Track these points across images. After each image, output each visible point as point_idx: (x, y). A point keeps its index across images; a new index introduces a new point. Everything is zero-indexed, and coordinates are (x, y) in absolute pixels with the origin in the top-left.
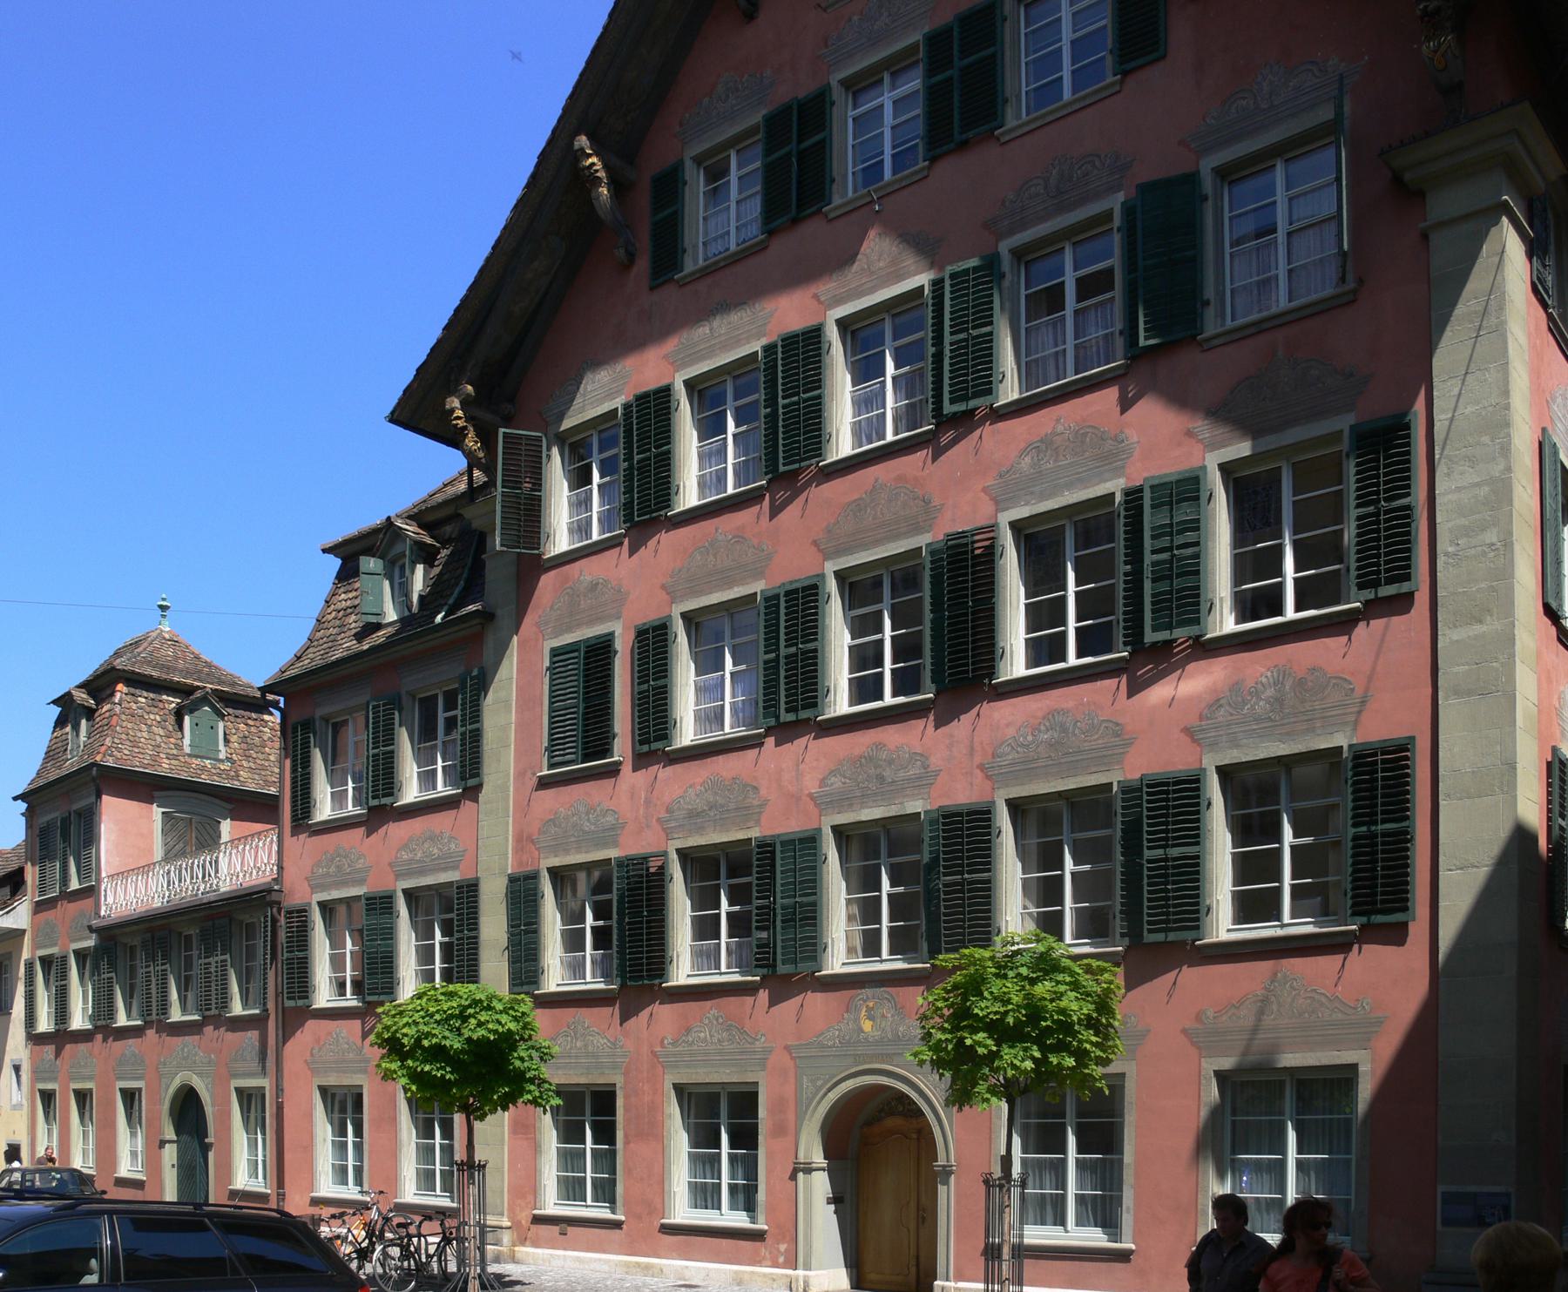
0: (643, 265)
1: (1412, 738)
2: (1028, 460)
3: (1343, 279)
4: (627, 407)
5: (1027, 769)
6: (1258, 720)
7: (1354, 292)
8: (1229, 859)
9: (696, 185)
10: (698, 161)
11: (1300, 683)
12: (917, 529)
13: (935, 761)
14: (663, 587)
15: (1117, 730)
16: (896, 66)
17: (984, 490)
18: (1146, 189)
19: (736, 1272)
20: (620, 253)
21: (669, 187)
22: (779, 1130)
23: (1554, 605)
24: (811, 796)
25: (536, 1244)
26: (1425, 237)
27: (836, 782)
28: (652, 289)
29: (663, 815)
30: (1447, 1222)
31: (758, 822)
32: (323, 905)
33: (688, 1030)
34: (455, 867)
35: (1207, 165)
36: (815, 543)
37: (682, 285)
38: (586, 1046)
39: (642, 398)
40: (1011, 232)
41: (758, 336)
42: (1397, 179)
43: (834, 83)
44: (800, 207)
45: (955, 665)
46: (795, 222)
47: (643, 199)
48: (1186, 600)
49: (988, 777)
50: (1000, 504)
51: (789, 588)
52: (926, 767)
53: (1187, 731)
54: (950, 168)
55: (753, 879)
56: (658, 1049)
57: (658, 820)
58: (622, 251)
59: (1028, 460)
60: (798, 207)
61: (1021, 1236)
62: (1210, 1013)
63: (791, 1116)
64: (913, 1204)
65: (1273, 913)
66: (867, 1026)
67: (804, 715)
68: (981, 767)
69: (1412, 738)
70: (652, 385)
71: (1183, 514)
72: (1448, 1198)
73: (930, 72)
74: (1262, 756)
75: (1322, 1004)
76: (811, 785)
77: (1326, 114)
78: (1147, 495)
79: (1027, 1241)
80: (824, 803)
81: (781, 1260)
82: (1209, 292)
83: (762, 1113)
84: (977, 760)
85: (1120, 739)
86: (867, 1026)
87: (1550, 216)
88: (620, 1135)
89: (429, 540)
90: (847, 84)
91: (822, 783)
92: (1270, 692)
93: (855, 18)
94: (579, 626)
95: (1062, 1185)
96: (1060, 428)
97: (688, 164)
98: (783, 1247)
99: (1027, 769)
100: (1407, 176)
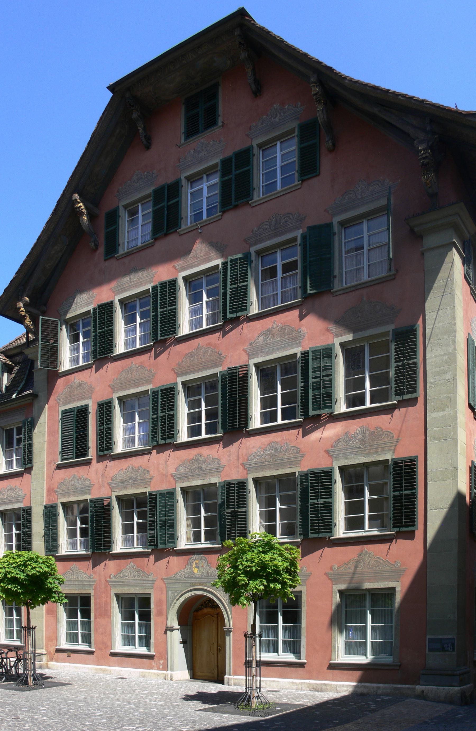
0: (101, 250)
2: (262, 338)
3: (390, 270)
7: (395, 275)
9: (124, 217)
10: (125, 207)
11: (372, 433)
15: (298, 451)
16: (209, 172)
17: (244, 350)
18: (310, 229)
19: (142, 672)
21: (113, 218)
24: (171, 475)
26: (423, 254)
27: (182, 469)
28: (105, 260)
30: (430, 650)
31: (149, 485)
33: (121, 571)
35: (336, 220)
36: (173, 370)
39: (101, 307)
40: (256, 244)
41: (150, 282)
42: (412, 231)
43: (183, 178)
46: (166, 235)
47: (102, 222)
49: (245, 469)
50: (250, 356)
53: (327, 452)
56: (108, 579)
57: (108, 483)
59: (262, 338)
60: (168, 199)
63: (164, 608)
66: (196, 570)
68: (242, 465)
69: (417, 457)
70: (105, 301)
71: (325, 363)
72: (431, 641)
73: (223, 175)
75: (381, 563)
77: (383, 202)
80: (177, 478)
81: (161, 667)
82: (336, 272)
84: (241, 461)
86: (196, 570)
90: (188, 178)
91: (176, 469)
92: (360, 436)
93: (192, 151)
94: (74, 401)
96: (275, 326)
98: (162, 662)
100: (416, 229)
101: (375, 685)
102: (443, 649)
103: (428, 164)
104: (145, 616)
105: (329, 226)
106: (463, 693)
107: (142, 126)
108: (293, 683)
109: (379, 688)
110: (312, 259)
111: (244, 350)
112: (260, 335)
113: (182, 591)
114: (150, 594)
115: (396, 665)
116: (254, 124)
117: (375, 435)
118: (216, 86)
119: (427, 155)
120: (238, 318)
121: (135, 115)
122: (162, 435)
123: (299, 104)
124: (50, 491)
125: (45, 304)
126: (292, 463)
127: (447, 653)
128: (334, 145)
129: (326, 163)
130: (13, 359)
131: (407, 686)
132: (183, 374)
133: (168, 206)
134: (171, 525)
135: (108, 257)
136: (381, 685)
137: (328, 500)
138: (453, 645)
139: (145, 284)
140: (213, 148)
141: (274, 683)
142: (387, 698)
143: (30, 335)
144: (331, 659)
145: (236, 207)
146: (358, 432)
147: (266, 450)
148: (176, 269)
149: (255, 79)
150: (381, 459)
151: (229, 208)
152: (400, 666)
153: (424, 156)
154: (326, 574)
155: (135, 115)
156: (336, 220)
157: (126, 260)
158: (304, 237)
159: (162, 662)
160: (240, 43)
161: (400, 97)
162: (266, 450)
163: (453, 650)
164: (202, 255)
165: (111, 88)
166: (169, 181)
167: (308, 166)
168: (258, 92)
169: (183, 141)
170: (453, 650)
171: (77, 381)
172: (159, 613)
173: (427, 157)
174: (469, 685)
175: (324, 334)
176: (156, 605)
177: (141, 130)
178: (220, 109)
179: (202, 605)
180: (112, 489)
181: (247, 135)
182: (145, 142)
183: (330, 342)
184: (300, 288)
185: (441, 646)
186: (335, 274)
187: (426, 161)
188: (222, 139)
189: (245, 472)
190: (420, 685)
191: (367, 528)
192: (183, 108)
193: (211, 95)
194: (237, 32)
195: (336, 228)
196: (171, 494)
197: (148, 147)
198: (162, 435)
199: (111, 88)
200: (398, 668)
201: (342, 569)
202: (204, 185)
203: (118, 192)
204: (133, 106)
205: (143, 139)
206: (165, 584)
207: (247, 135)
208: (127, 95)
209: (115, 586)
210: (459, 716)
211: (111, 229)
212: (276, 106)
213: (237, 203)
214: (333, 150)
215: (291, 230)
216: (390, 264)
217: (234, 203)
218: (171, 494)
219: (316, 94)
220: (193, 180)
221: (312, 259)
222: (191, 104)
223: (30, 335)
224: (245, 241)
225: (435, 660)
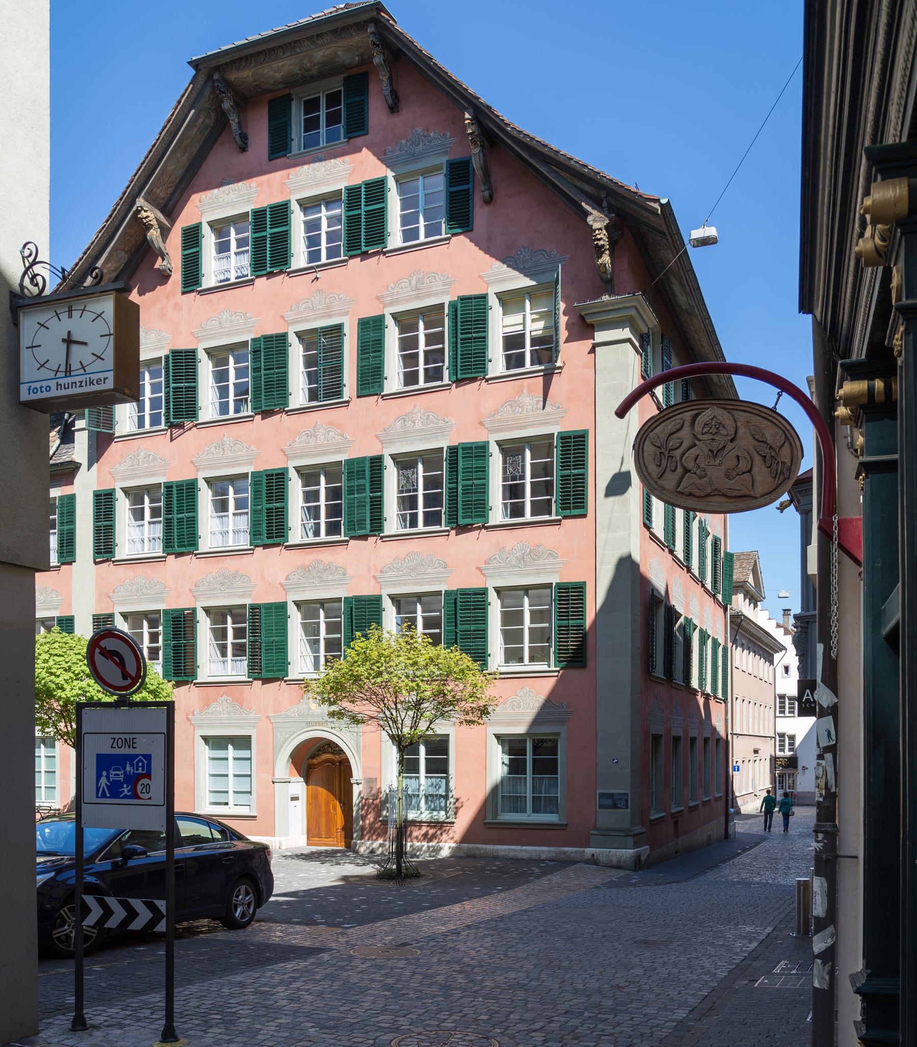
1: (585, 583)
2: (399, 424)
8: (499, 614)
12: (340, 451)
17: (376, 436)
23: (648, 522)
24: (280, 584)
26: (593, 350)
28: (183, 293)
30: (601, 807)
33: (208, 706)
48: (480, 508)
49: (379, 583)
51: (269, 473)
53: (479, 569)
55: (246, 625)
57: (190, 590)
59: (399, 424)
61: (49, 742)
65: (521, 364)
67: (277, 540)
69: (585, 583)
72: (602, 795)
78: (460, 452)
79: (42, 751)
91: (287, 578)
101: (538, 848)
102: (615, 806)
106: (638, 857)
107: (237, 120)
112: (397, 420)
113: (294, 733)
119: (602, 236)
122: (270, 529)
128: (491, 196)
131: (575, 849)
132: (296, 457)
134: (281, 648)
138: (627, 801)
142: (552, 863)
149: (391, 91)
155: (227, 105)
160: (374, 44)
162: (403, 562)
163: (627, 808)
164: (321, 307)
170: (627, 808)
175: (476, 428)
179: (319, 750)
189: (378, 587)
194: (371, 29)
196: (281, 607)
198: (270, 529)
202: (324, 214)
203: (200, 201)
204: (224, 93)
205: (238, 138)
206: (272, 723)
208: (216, 76)
209: (201, 726)
210: (634, 881)
218: (281, 607)
225: (608, 818)
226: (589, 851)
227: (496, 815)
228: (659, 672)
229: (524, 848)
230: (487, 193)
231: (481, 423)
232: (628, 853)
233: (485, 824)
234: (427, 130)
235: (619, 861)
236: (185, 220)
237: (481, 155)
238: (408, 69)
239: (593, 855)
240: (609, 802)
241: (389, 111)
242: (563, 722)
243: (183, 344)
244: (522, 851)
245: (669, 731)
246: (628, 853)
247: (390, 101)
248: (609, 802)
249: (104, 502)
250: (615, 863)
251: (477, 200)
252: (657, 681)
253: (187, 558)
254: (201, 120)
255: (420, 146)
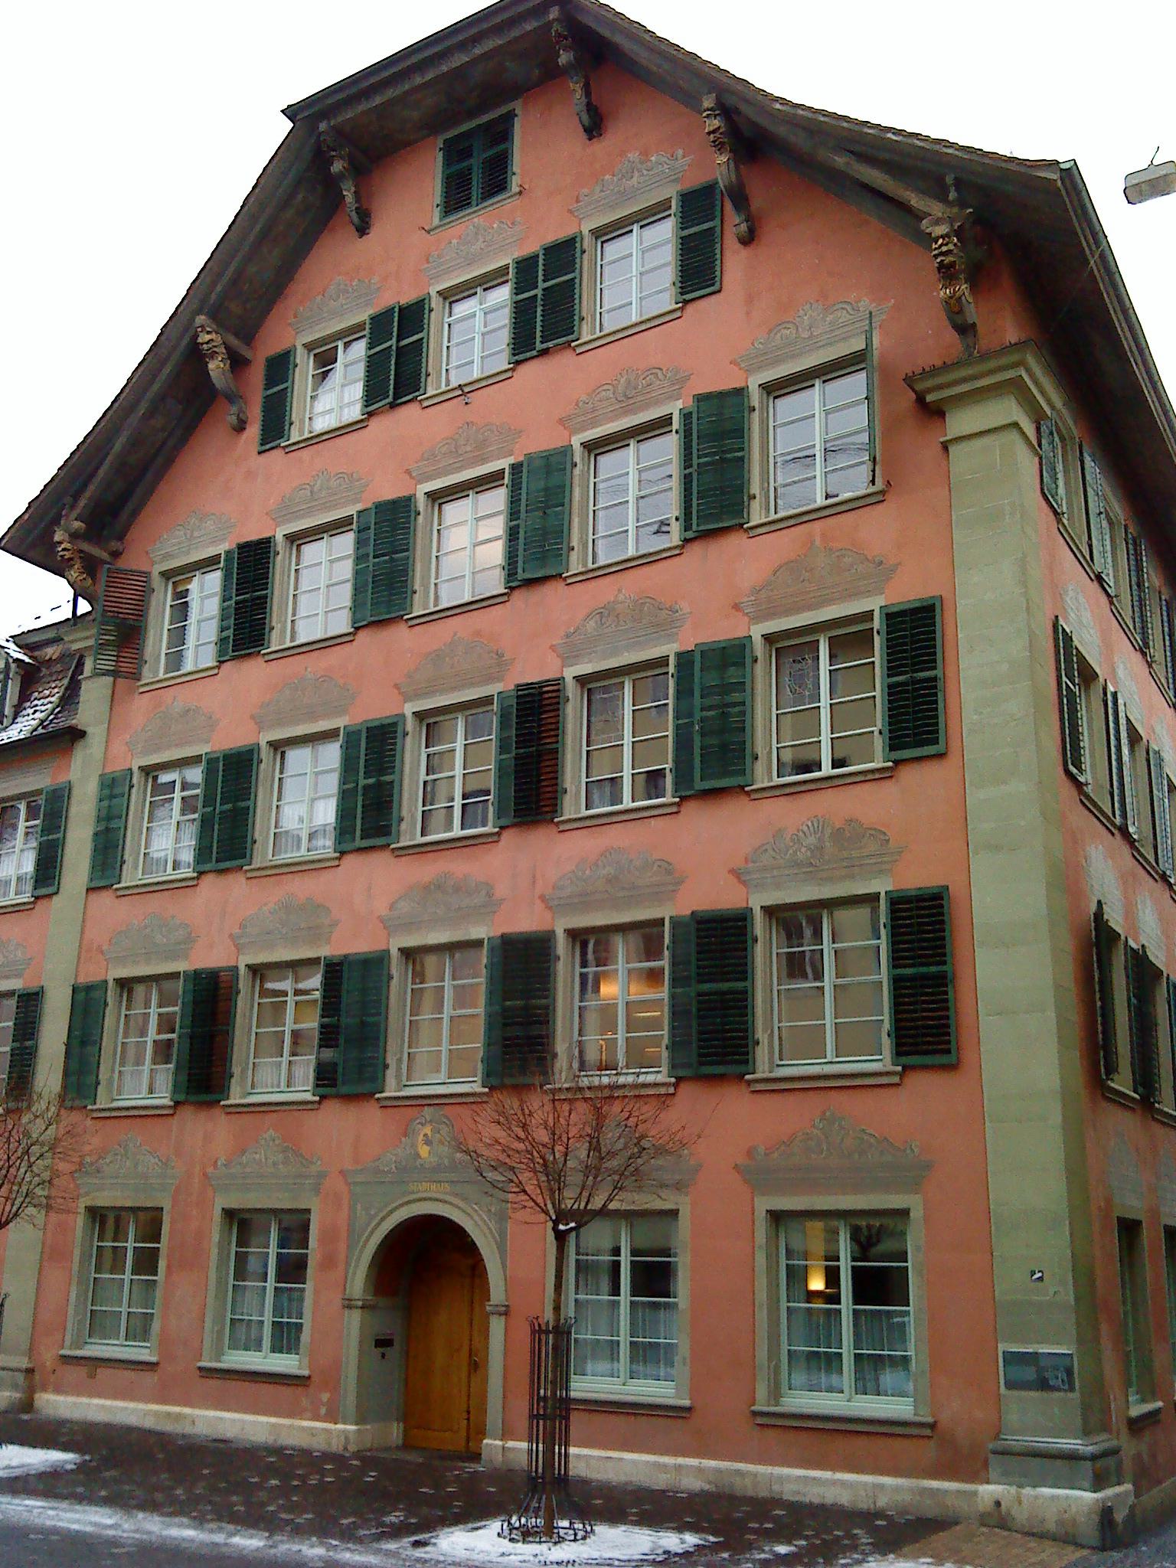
0: (254, 431)
2: (592, 623)
3: (873, 482)
4: (228, 553)
5: (585, 902)
6: (797, 864)
7: (882, 492)
9: (305, 366)
10: (309, 347)
11: (838, 835)
12: (490, 679)
13: (501, 890)
14: (252, 717)
15: (667, 868)
16: (488, 281)
17: (552, 647)
18: (700, 399)
19: (273, 1425)
20: (233, 419)
21: (280, 367)
22: (501, 663)
25: (58, 1390)
26: (945, 446)
27: (404, 907)
29: (236, 931)
30: (1010, 1385)
31: (328, 941)
32: (573, 934)
33: (243, 1152)
34: (17, 976)
35: (754, 383)
36: (396, 686)
37: (288, 450)
38: (136, 1166)
39: (243, 547)
40: (583, 429)
41: (355, 501)
42: (920, 400)
43: (433, 294)
44: (396, 398)
45: (529, 791)
46: (393, 406)
47: (257, 374)
49: (550, 908)
50: (567, 660)
52: (489, 895)
54: (532, 371)
56: (210, 1170)
58: (234, 418)
59: (592, 623)
60: (398, 336)
62: (761, 1149)
63: (342, 1247)
64: (465, 1350)
66: (424, 1151)
68: (542, 898)
70: (254, 537)
71: (732, 675)
72: (1011, 1358)
73: (518, 290)
74: (803, 899)
75: (871, 1145)
76: (381, 907)
77: (858, 344)
80: (390, 926)
81: (323, 1411)
82: (755, 488)
83: (313, 1242)
84: (538, 892)
85: (672, 879)
86: (424, 1151)
87: (1057, 439)
88: (162, 1264)
89: (27, 660)
90: (444, 294)
92: (812, 840)
93: (455, 241)
94: (169, 747)
95: (614, 1329)
96: (621, 597)
97: (300, 351)
98: (325, 1397)
99: (585, 902)
100: (929, 398)
102: (1043, 1385)
103: (952, 265)
104: (292, 1270)
105: (740, 392)
106: (1106, 1514)
108: (656, 1464)
109: (881, 1487)
110: (702, 460)
111: (552, 647)
114: (308, 1211)
115: (922, 1425)
116: (585, 191)
117: (848, 835)
118: (510, 116)
119: (951, 247)
120: (548, 349)
121: (337, 167)
123: (680, 152)
124: (84, 951)
125: (121, 538)
126: (658, 895)
127: (1057, 1395)
129: (735, 264)
130: (36, 654)
132: (417, 695)
133: (398, 348)
135: (268, 447)
136: (887, 1480)
137: (740, 985)
138: (1069, 1372)
139: (344, 505)
140: (502, 233)
141: (610, 1464)
143: (81, 601)
144: (754, 1398)
145: (544, 353)
146: (805, 829)
147: (635, 855)
148: (411, 477)
150: (860, 892)
151: (528, 355)
152: (933, 1426)
153: (944, 249)
154: (736, 1167)
156: (754, 383)
157: (305, 454)
158: (686, 416)
159: (325, 1397)
161: (890, 135)
163: (1072, 1389)
164: (469, 448)
165: (290, 112)
166: (405, 300)
167: (697, 273)
168: (594, 128)
169: (436, 221)
170: (1072, 1389)
171: (178, 706)
172: (328, 1263)
173: (949, 252)
174: (1118, 1489)
176: (321, 1241)
177: (349, 196)
178: (518, 161)
180: (239, 949)
181: (570, 211)
182: (356, 219)
183: (741, 633)
184: (677, 519)
185: (1037, 1375)
186: (752, 492)
187: (948, 259)
188: (518, 219)
189: (548, 915)
190: (988, 1483)
191: (830, 1055)
192: (440, 156)
193: (500, 133)
195: (755, 397)
197: (363, 230)
199: (290, 112)
200: (928, 1432)
201: (776, 1155)
206: (348, 1184)
207: (570, 211)
211: (275, 389)
212: (634, 156)
213: (545, 346)
214: (748, 240)
215: (658, 402)
216: (874, 471)
217: (539, 346)
219: (713, 132)
220: (453, 295)
221: (702, 460)
222: (456, 152)
223: (81, 601)
224: (561, 421)
225: (1041, 1421)
226: (989, 1491)
227: (776, 1395)
228: (1122, 1083)
229: (839, 1476)
230: (744, 227)
231: (736, 607)
232: (1081, 1499)
233: (755, 1414)
234: (645, 153)
235: (1060, 1523)
236: (269, 345)
237: (732, 165)
238: (619, 69)
239: (998, 1504)
240: (1029, 1373)
241: (585, 136)
242: (915, 1185)
243: (253, 533)
244: (834, 1483)
245: (1154, 1213)
246: (1081, 1499)
247: (585, 117)
248: (1029, 1373)
249: (114, 788)
250: (1051, 1526)
251: (731, 242)
252: (1118, 1099)
253: (231, 878)
254: (300, 197)
255: (635, 179)
